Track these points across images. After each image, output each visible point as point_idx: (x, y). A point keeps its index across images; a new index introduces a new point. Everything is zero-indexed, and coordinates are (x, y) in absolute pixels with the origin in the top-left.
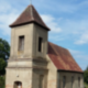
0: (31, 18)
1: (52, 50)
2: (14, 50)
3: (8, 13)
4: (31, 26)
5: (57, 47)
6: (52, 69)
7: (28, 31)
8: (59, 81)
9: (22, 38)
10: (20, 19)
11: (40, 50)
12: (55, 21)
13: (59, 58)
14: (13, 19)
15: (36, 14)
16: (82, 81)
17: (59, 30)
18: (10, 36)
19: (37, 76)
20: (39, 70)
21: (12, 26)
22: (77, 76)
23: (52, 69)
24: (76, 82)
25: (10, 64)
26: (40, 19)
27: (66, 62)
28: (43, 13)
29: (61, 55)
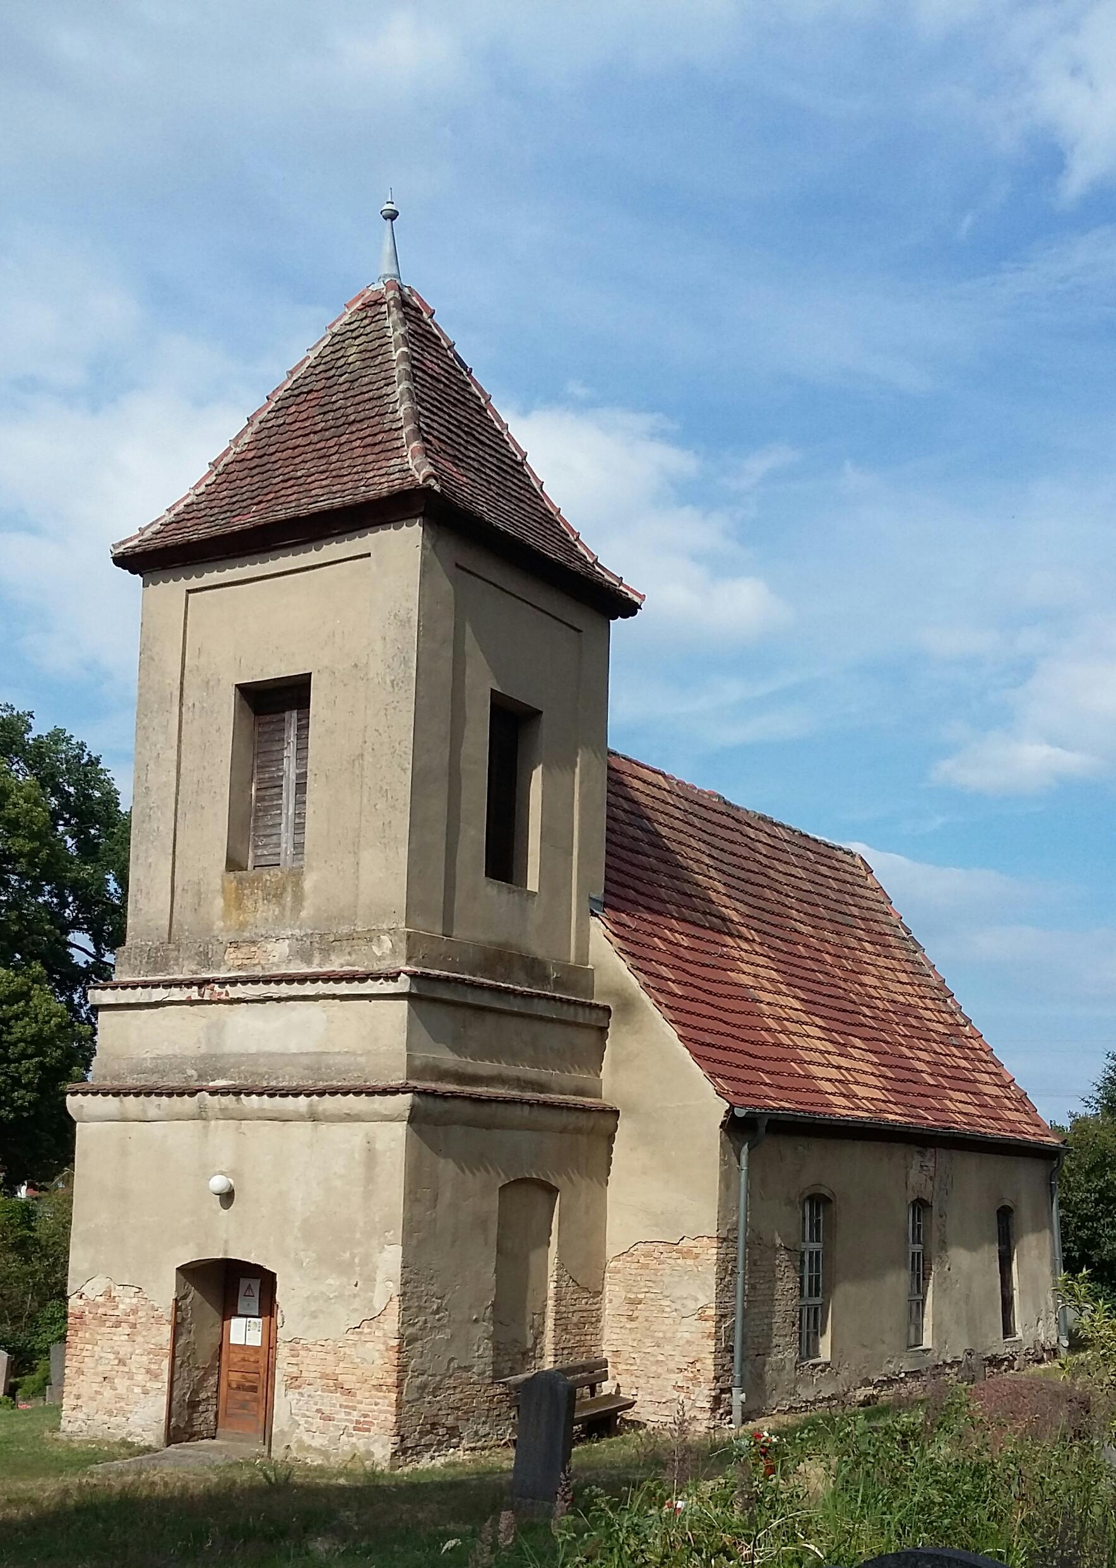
0: (395, 456)
1: (652, 857)
2: (171, 871)
3: (104, 384)
4: (402, 546)
5: (720, 819)
6: (663, 1096)
7: (358, 614)
8: (748, 1262)
9: (274, 704)
10: (235, 473)
11: (503, 860)
12: (691, 494)
13: (752, 969)
14: (164, 470)
15: (452, 404)
16: (1037, 1257)
17: (743, 604)
18: (122, 681)
19: (475, 1195)
20: (499, 1124)
21: (148, 560)
22: (972, 1184)
23: (663, 1096)
24: (968, 1265)
25: (131, 1034)
26: (511, 469)
27: (843, 1017)
28: (546, 394)
29: (770, 924)
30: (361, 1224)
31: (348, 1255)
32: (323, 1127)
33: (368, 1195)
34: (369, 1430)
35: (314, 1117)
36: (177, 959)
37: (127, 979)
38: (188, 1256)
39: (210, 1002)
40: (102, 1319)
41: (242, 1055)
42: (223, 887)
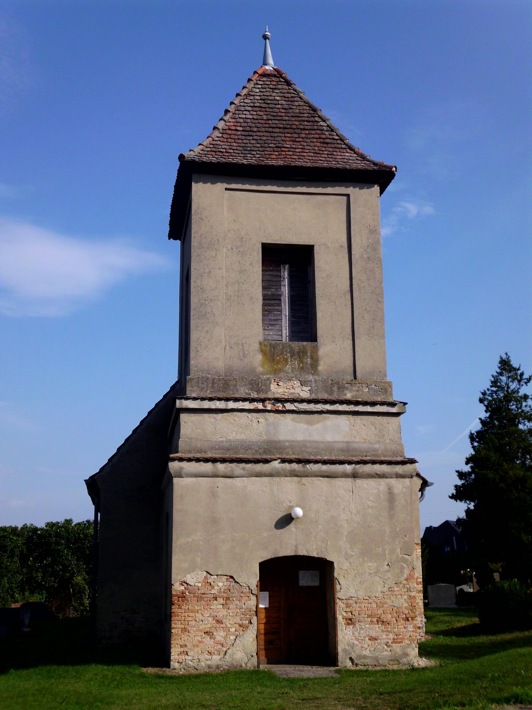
30: (388, 532)
31: (380, 549)
32: (359, 481)
33: (391, 516)
34: (402, 642)
35: (355, 476)
36: (235, 386)
37: (194, 395)
38: (267, 555)
39: (269, 411)
40: (200, 598)
41: (293, 441)
42: (261, 349)
